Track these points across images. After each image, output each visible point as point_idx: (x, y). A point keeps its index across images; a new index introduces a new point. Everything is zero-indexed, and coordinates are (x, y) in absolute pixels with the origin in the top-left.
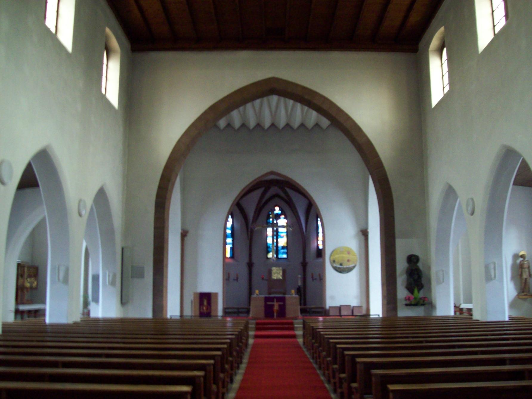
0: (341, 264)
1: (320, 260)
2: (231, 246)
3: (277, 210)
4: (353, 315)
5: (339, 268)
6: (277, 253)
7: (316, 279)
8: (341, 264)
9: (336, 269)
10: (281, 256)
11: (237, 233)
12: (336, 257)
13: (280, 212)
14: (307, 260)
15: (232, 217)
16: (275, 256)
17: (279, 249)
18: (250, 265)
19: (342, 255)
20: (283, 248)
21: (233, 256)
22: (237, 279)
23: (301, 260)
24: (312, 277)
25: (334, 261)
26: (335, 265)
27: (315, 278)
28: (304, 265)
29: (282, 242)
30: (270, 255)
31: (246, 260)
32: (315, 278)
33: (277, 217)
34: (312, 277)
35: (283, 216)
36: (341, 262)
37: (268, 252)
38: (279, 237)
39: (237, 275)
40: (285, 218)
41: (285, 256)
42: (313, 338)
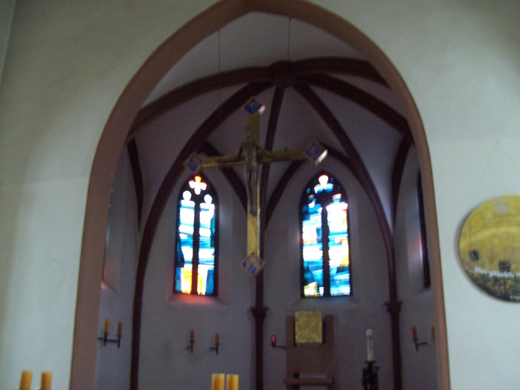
0: (504, 266)
1: (429, 293)
2: (212, 267)
3: (324, 184)
4: (118, 342)
5: (496, 280)
6: (327, 281)
7: (425, 344)
8: (504, 266)
9: (484, 285)
10: (334, 291)
11: (225, 237)
12: (481, 236)
13: (330, 186)
14: (402, 296)
15: (215, 201)
16: (322, 290)
17: (333, 272)
18: (259, 313)
19: (503, 229)
20: (340, 270)
21: (214, 293)
22: (216, 349)
23: (386, 297)
24: (415, 339)
25: (475, 255)
26: (478, 270)
27: (421, 340)
28: (394, 308)
29: (340, 255)
30: (310, 290)
31: (250, 302)
32: (421, 340)
33: (324, 199)
34: (415, 339)
35: (338, 196)
36: (502, 257)
37: (304, 282)
38: (330, 243)
39: (217, 337)
40: (343, 199)
41: (346, 290)
42: (495, 215)
